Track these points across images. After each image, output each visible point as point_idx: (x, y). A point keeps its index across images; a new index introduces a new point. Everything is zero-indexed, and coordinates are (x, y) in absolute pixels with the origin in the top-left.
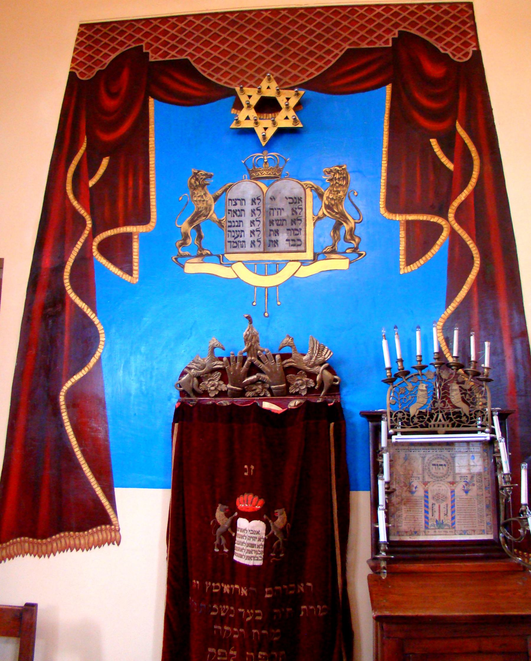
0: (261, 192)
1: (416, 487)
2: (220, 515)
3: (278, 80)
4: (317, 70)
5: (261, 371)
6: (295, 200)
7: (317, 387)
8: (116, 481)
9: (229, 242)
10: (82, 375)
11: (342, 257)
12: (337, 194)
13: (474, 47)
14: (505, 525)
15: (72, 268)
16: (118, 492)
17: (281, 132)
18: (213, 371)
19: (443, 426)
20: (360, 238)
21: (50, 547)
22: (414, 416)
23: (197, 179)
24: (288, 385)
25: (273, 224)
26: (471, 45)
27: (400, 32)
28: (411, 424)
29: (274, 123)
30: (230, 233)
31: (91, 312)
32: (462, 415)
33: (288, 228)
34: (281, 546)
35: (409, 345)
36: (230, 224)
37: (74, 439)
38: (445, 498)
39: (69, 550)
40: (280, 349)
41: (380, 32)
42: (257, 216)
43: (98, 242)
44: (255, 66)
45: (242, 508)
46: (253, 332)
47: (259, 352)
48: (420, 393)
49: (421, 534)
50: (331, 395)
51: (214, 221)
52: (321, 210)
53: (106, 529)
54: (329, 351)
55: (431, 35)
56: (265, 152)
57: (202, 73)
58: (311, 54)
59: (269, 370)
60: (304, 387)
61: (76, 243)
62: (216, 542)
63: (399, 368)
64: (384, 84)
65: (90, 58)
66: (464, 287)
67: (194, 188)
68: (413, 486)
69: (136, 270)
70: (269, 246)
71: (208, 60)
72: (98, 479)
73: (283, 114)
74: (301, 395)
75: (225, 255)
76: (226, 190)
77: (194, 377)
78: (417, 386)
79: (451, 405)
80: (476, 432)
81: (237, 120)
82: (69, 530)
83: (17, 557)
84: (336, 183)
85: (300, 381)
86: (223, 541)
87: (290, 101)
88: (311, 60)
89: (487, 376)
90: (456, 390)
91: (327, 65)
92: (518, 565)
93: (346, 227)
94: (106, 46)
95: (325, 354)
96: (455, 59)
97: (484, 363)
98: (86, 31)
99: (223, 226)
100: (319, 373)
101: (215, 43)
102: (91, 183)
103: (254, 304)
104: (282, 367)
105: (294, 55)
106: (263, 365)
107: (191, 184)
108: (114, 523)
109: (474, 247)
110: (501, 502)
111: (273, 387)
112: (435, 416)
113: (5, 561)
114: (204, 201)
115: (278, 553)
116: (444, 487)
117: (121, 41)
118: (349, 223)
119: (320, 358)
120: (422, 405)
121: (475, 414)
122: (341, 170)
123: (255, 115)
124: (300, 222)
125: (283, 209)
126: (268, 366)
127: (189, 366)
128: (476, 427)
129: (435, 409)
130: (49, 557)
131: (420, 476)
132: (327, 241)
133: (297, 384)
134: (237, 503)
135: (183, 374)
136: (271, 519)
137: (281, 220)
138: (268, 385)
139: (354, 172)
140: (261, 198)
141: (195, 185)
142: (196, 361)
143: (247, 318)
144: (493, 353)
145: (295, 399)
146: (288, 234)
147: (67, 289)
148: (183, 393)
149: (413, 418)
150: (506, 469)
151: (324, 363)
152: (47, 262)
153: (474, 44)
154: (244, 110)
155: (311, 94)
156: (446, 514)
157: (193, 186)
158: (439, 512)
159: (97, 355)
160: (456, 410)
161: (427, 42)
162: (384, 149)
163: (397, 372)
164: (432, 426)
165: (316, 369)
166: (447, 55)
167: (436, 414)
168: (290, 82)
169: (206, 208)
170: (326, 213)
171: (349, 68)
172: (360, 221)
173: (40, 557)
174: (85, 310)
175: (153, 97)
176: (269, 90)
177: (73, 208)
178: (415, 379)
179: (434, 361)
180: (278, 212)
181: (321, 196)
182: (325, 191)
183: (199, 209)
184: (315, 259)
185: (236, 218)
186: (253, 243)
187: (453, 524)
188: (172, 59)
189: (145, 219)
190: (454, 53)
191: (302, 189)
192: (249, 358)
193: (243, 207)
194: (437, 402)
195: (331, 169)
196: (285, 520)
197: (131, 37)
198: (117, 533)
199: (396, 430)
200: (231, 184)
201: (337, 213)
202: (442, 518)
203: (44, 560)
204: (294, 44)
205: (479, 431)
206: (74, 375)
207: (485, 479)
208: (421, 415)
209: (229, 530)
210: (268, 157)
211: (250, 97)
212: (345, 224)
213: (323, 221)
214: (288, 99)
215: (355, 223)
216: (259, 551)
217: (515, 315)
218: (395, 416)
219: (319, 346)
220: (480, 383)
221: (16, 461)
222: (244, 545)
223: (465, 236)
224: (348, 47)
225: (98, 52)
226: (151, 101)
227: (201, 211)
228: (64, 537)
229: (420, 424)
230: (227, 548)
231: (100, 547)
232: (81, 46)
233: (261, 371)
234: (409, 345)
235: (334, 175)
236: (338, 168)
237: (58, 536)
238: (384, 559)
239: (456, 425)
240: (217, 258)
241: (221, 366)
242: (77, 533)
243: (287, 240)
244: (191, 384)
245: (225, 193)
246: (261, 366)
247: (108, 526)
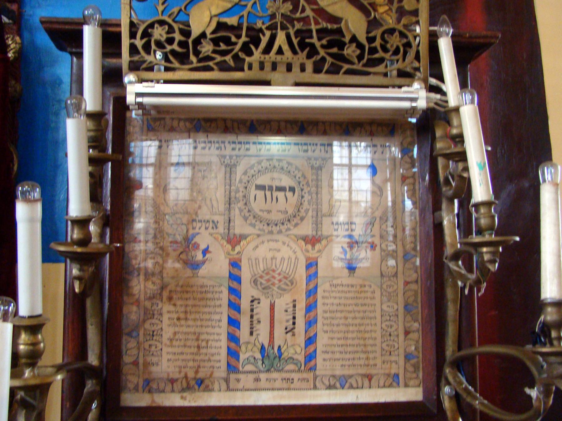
22: (203, 35)
28: (193, 58)
32: (347, 39)
49: (216, 386)
79: (313, 10)
110: (449, 293)
112: (264, 40)
116: (285, 252)
121: (383, 38)
131: (221, 220)
149: (198, 41)
156: (291, 331)
164: (256, 66)
167: (268, 34)
187: (310, 357)
202: (278, 342)
229: (219, 58)
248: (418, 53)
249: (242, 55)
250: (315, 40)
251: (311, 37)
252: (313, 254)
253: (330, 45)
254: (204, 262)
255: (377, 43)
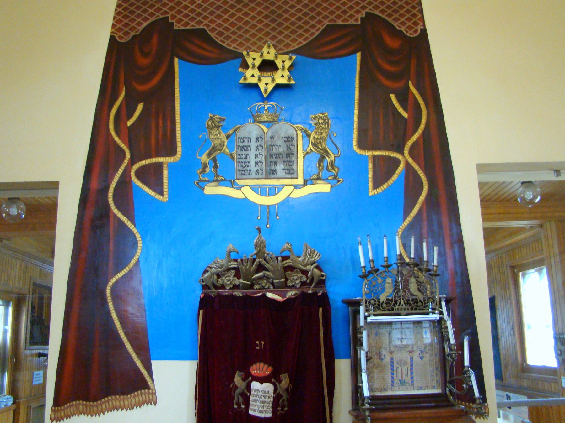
0: (263, 134)
1: (384, 356)
2: (238, 379)
3: (275, 47)
4: (305, 40)
5: (266, 269)
6: (289, 139)
7: (308, 281)
8: (152, 356)
9: (238, 170)
10: (124, 273)
11: (326, 183)
12: (321, 135)
13: (422, 26)
14: (451, 382)
15: (115, 190)
16: (155, 364)
17: (278, 87)
18: (229, 269)
19: (405, 309)
20: (339, 169)
21: (100, 408)
22: (383, 302)
23: (213, 122)
24: (287, 279)
25: (272, 157)
26: (419, 24)
27: (366, 13)
28: (381, 308)
29: (273, 80)
30: (239, 164)
31: (131, 224)
32: (419, 301)
33: (284, 160)
34: (285, 402)
35: (377, 249)
36: (239, 157)
37: (119, 323)
38: (406, 363)
39: (116, 410)
40: (282, 252)
41: (352, 12)
42: (260, 151)
43: (135, 170)
44: (257, 35)
45: (255, 373)
46: (262, 239)
47: (265, 255)
48: (387, 285)
49: (389, 390)
50: (319, 287)
51: (226, 154)
52: (309, 147)
53: (145, 393)
54: (319, 254)
55: (389, 15)
56: (266, 102)
57: (215, 39)
58: (300, 27)
59: (272, 269)
60: (298, 281)
61: (118, 170)
62: (235, 401)
63: (371, 266)
64: (355, 52)
65: (126, 25)
66: (417, 205)
67: (210, 128)
68: (382, 354)
69: (166, 191)
70: (270, 174)
71: (220, 29)
72: (138, 354)
73: (279, 73)
74: (296, 287)
75: (236, 180)
76: (235, 131)
77: (214, 274)
78: (385, 280)
79: (410, 294)
80: (428, 314)
81: (245, 77)
82: (116, 394)
83: (73, 416)
84: (320, 126)
85: (296, 277)
86: (241, 400)
87: (285, 63)
88: (300, 32)
89: (436, 272)
90: (413, 283)
91: (312, 36)
92: (462, 410)
93: (328, 160)
94: (139, 16)
95: (315, 257)
96: (408, 35)
97: (434, 262)
98: (123, 4)
99: (234, 159)
100: (310, 270)
101: (226, 16)
102: (129, 123)
103: (259, 218)
104: (282, 267)
105: (287, 28)
106: (268, 265)
107: (208, 125)
108: (151, 388)
109: (423, 176)
110: (447, 365)
111: (275, 281)
112: (398, 303)
113: (63, 420)
114: (219, 138)
115: (283, 407)
116: (404, 355)
117: (151, 12)
118: (330, 157)
119: (312, 259)
120: (389, 294)
121: (427, 300)
122: (323, 117)
123: (259, 73)
124: (293, 155)
125: (280, 146)
126: (272, 266)
127: (210, 266)
128: (429, 310)
129: (398, 297)
130: (99, 415)
131: (388, 347)
132: (314, 170)
133: (293, 279)
134: (251, 370)
135: (206, 271)
136: (277, 382)
137: (278, 154)
138: (271, 280)
139: (334, 118)
140: (263, 137)
141: (211, 126)
142: (216, 262)
143: (257, 229)
144: (439, 254)
145: (291, 290)
146: (284, 164)
147: (111, 206)
148: (205, 287)
149: (382, 304)
150: (452, 341)
151: (314, 263)
152: (95, 184)
153: (421, 24)
154: (250, 69)
155: (303, 59)
156: (407, 375)
157: (210, 126)
158: (402, 373)
159: (136, 257)
160: (414, 297)
161: (387, 21)
162: (356, 101)
163: (370, 269)
164: (397, 309)
165: (308, 267)
166: (401, 31)
167: (399, 301)
168: (284, 48)
169: (220, 144)
170: (312, 149)
171: (327, 39)
172: (338, 155)
173: (92, 416)
174: (126, 223)
175: (177, 57)
176: (269, 54)
177: (115, 142)
178: (384, 275)
179: (396, 261)
180: (276, 148)
181: (309, 136)
182: (312, 132)
183: (215, 145)
184: (305, 183)
185: (244, 152)
186: (257, 171)
187: (412, 382)
188: (192, 28)
189: (172, 152)
190: (407, 30)
191: (295, 131)
192: (258, 260)
193: (249, 144)
194: (399, 291)
195: (316, 115)
196: (288, 382)
197: (158, 10)
198: (154, 396)
199: (369, 313)
200: (240, 126)
201: (321, 149)
202: (404, 378)
203: (95, 418)
204: (287, 20)
205: (431, 312)
206: (117, 273)
207: (435, 348)
208: (388, 301)
209: (245, 391)
210: (268, 106)
211: (254, 59)
212: (327, 158)
213: (310, 155)
214: (283, 62)
215: (335, 157)
216: (269, 406)
217: (454, 226)
218: (369, 302)
219: (311, 250)
220: (431, 277)
221: (72, 341)
222: (257, 402)
223: (416, 167)
224: (327, 23)
225: (133, 20)
226: (176, 60)
227: (217, 146)
228: (112, 400)
229: (387, 308)
230: (244, 404)
231: (140, 407)
232: (119, 16)
233: (266, 269)
234: (377, 249)
235: (318, 121)
236: (321, 115)
237: (106, 399)
238: (368, 409)
239: (414, 308)
240: (230, 183)
241: (236, 266)
242: (122, 397)
243: (283, 170)
244: (212, 280)
245: (235, 133)
246: (267, 265)
247: (147, 391)
248: (436, 303)
249: (393, 307)
250: (411, 302)
251: (410, 301)
252: (412, 355)
253: (414, 303)
254: (384, 358)
255: (426, 301)
